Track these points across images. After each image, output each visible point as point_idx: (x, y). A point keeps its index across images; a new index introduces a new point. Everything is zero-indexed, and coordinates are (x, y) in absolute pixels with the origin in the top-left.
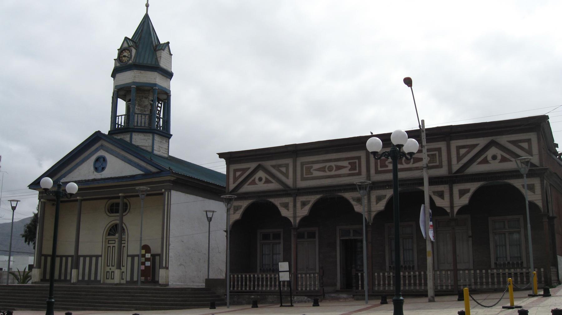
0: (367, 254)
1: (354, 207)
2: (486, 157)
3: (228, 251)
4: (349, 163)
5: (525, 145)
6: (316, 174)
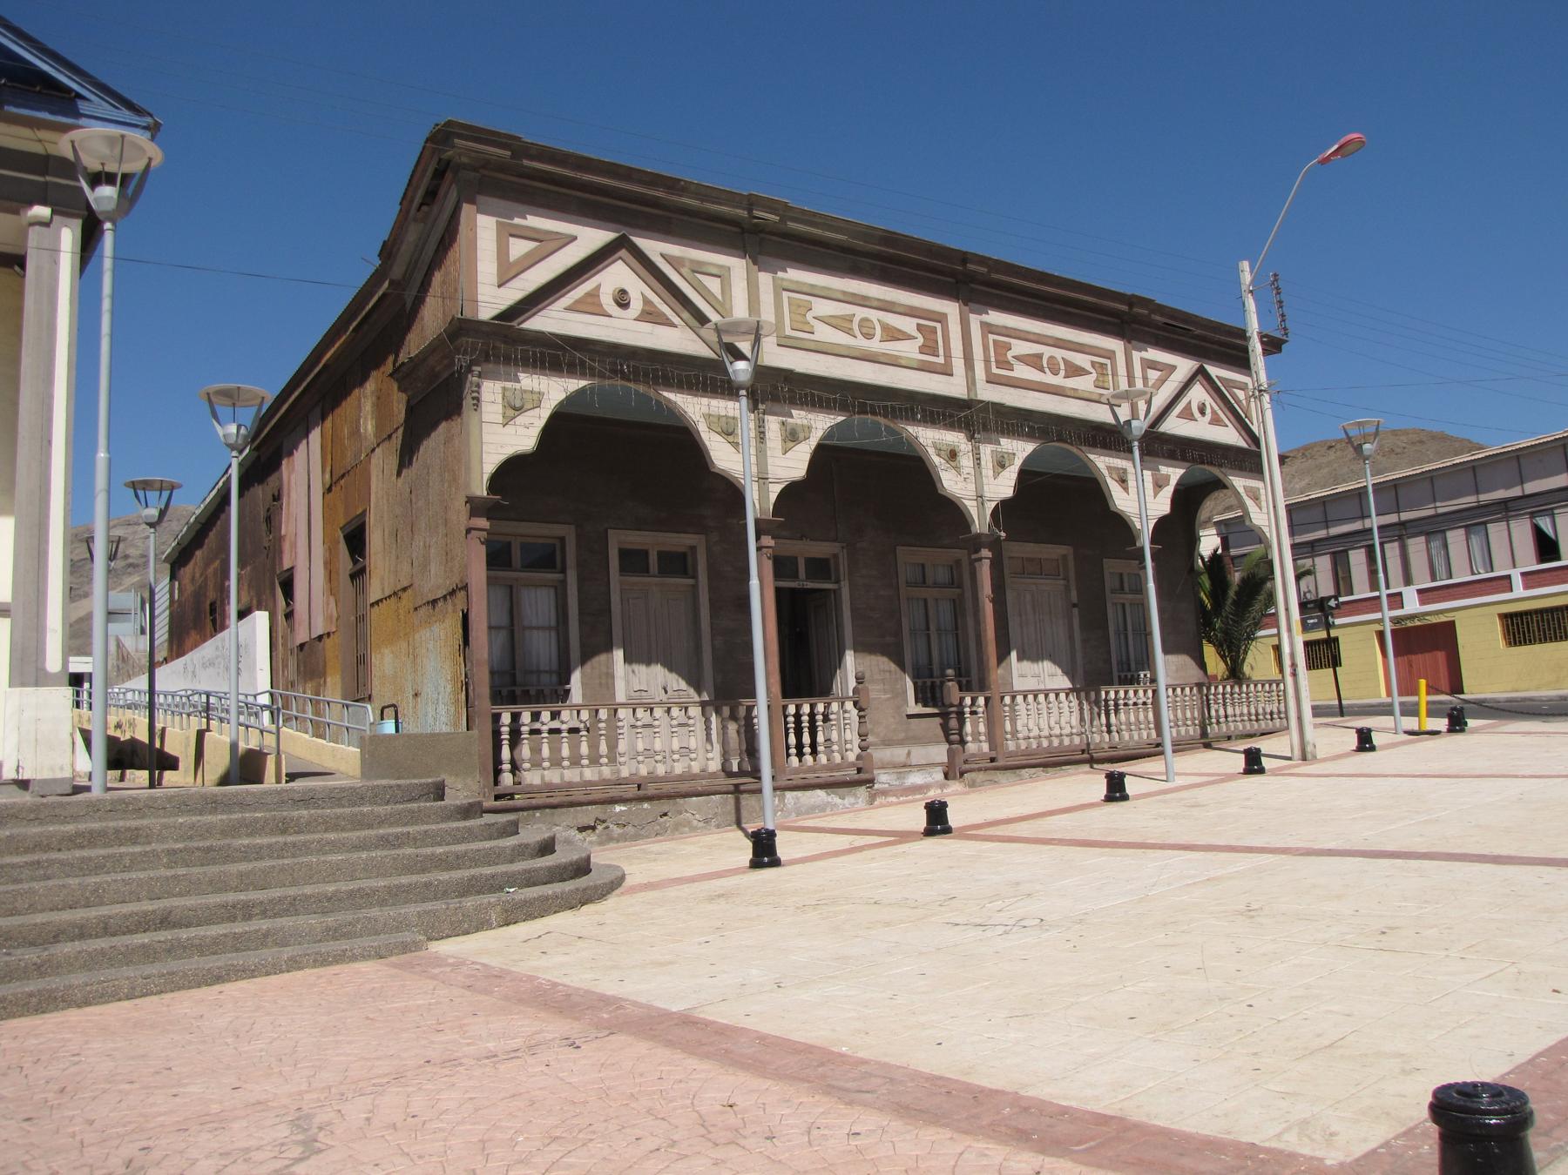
0: (978, 622)
3: (541, 541)
5: (713, 285)
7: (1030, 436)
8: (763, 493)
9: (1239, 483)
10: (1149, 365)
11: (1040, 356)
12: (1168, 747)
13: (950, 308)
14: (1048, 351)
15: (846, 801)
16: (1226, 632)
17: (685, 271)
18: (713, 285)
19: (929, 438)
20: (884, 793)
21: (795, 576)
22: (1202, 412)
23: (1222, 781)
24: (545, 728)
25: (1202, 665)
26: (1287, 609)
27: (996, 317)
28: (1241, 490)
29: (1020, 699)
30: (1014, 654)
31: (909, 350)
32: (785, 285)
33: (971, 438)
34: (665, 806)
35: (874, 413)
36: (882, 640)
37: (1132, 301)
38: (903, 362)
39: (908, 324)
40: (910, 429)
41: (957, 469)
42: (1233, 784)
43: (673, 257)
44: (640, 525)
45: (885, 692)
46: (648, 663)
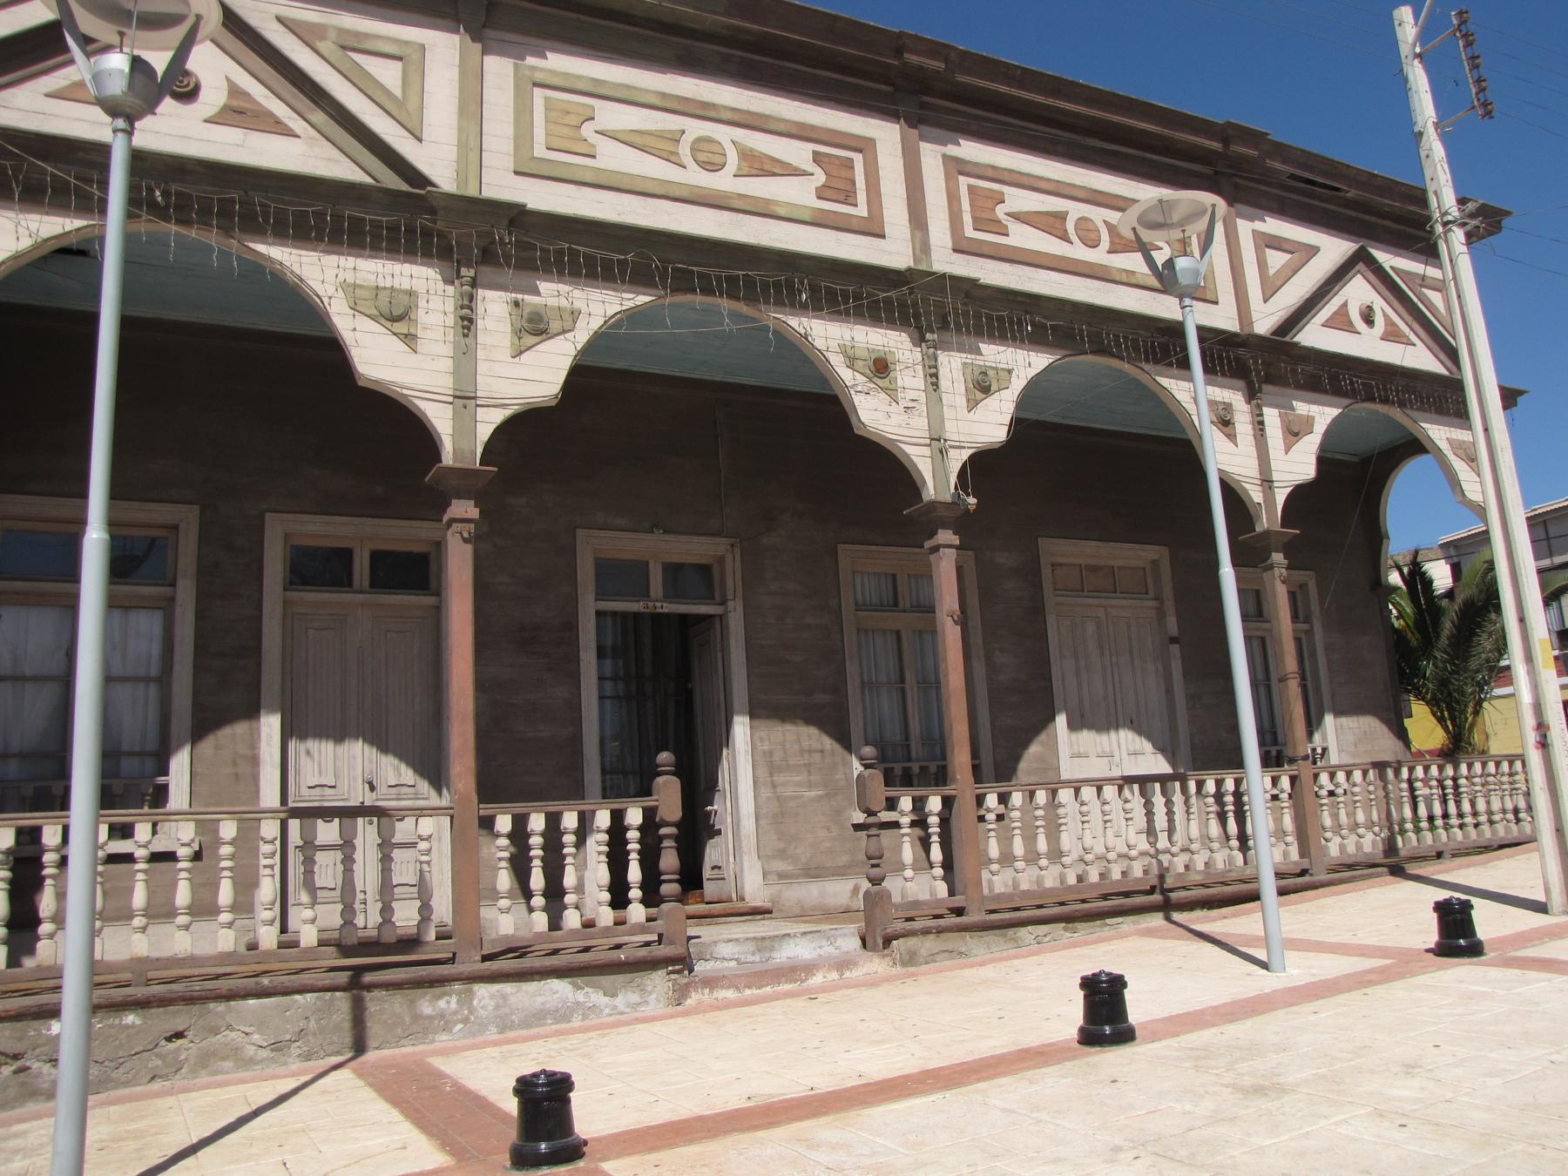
1: (858, 400)
2: (1345, 305)
4: (817, 158)
5: (388, 74)
6: (615, 159)
7: (1037, 340)
8: (465, 423)
9: (1438, 433)
10: (1276, 243)
11: (1061, 217)
12: (1268, 886)
13: (886, 134)
14: (1076, 210)
15: (620, 1001)
16: (1443, 683)
17: (325, 46)
18: (388, 74)
19: (830, 338)
20: (711, 982)
21: (645, 593)
22: (1369, 321)
23: (1383, 976)
24: (140, 853)
25: (1402, 735)
26: (1522, 620)
27: (972, 150)
28: (1444, 446)
29: (1065, 795)
30: (1061, 720)
31: (800, 193)
32: (539, 77)
33: (919, 340)
34: (178, 1018)
35: (707, 291)
36: (808, 694)
37: (1228, 133)
38: (782, 212)
39: (798, 153)
40: (793, 322)
41: (892, 393)
42: (1398, 991)
43: (293, 20)
44: (330, 505)
45: (810, 785)
46: (339, 737)
